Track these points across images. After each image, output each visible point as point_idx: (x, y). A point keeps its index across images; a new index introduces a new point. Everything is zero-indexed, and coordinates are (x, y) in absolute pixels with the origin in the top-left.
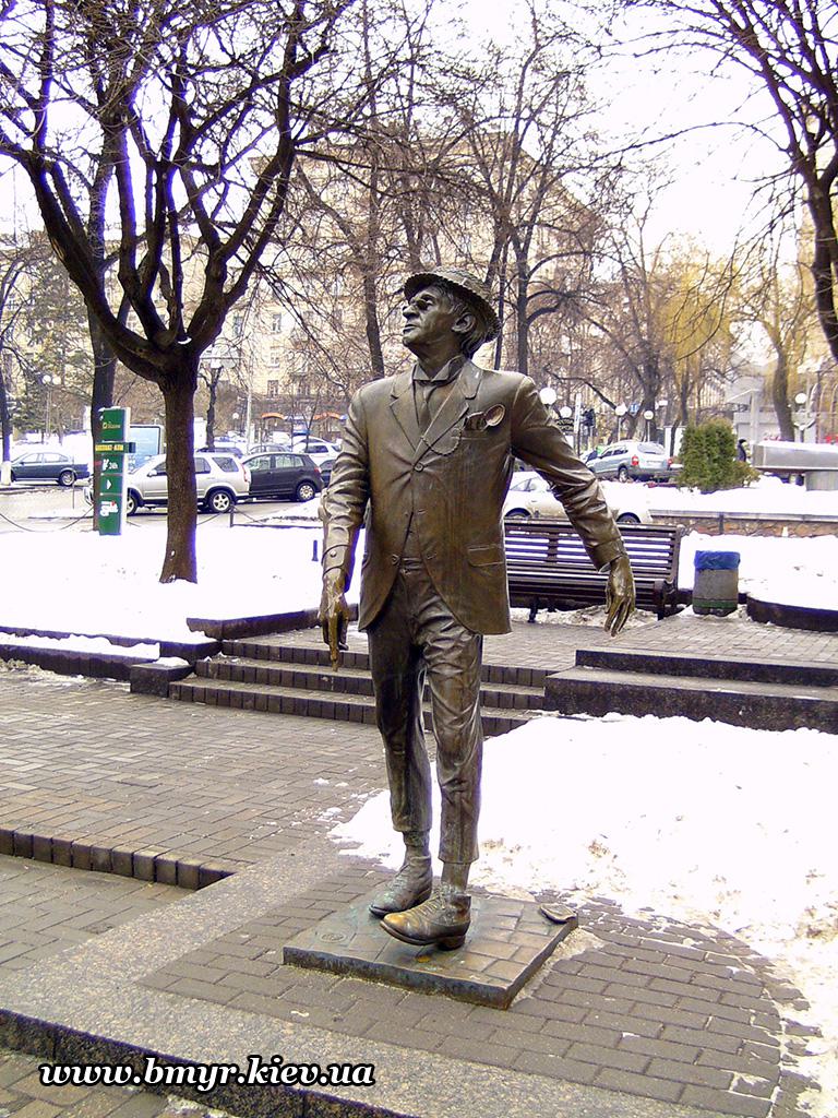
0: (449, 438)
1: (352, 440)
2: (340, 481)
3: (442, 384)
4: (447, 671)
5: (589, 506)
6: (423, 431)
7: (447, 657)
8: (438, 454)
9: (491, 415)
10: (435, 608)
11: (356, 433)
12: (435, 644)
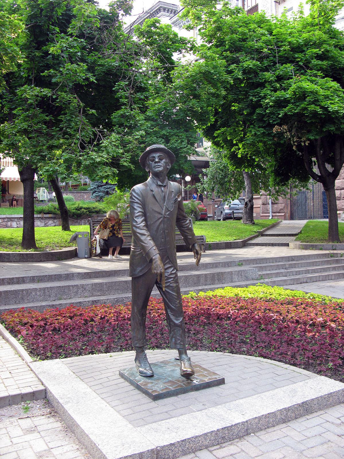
1: (140, 206)
11: (139, 202)
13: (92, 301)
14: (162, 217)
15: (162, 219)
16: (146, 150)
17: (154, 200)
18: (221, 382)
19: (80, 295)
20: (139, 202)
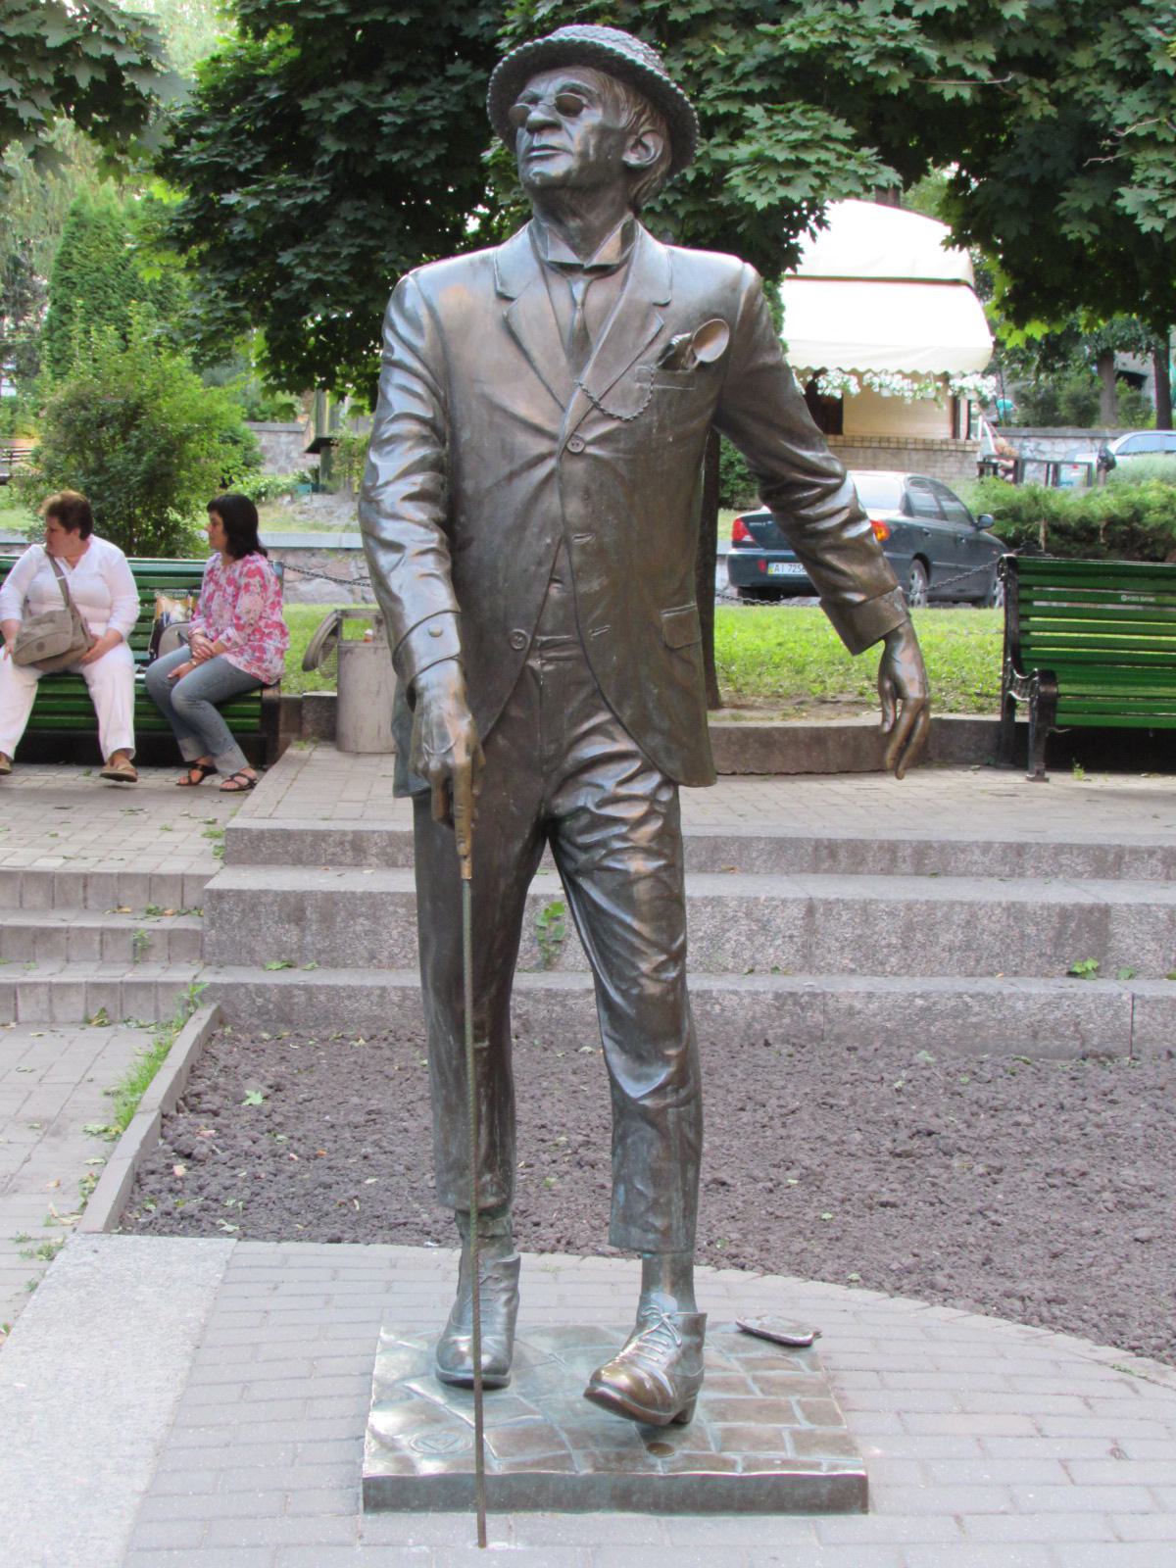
0: (629, 388)
1: (419, 388)
2: (406, 473)
3: (603, 271)
4: (638, 865)
5: (845, 525)
6: (578, 368)
7: (632, 836)
8: (611, 417)
9: (702, 339)
10: (598, 738)
11: (417, 365)
12: (610, 811)
13: (777, 996)
14: (550, 454)
15: (550, 464)
16: (553, 37)
17: (509, 352)
18: (847, 1496)
19: (734, 955)
20: (417, 365)
